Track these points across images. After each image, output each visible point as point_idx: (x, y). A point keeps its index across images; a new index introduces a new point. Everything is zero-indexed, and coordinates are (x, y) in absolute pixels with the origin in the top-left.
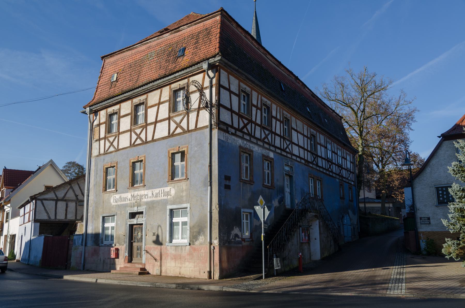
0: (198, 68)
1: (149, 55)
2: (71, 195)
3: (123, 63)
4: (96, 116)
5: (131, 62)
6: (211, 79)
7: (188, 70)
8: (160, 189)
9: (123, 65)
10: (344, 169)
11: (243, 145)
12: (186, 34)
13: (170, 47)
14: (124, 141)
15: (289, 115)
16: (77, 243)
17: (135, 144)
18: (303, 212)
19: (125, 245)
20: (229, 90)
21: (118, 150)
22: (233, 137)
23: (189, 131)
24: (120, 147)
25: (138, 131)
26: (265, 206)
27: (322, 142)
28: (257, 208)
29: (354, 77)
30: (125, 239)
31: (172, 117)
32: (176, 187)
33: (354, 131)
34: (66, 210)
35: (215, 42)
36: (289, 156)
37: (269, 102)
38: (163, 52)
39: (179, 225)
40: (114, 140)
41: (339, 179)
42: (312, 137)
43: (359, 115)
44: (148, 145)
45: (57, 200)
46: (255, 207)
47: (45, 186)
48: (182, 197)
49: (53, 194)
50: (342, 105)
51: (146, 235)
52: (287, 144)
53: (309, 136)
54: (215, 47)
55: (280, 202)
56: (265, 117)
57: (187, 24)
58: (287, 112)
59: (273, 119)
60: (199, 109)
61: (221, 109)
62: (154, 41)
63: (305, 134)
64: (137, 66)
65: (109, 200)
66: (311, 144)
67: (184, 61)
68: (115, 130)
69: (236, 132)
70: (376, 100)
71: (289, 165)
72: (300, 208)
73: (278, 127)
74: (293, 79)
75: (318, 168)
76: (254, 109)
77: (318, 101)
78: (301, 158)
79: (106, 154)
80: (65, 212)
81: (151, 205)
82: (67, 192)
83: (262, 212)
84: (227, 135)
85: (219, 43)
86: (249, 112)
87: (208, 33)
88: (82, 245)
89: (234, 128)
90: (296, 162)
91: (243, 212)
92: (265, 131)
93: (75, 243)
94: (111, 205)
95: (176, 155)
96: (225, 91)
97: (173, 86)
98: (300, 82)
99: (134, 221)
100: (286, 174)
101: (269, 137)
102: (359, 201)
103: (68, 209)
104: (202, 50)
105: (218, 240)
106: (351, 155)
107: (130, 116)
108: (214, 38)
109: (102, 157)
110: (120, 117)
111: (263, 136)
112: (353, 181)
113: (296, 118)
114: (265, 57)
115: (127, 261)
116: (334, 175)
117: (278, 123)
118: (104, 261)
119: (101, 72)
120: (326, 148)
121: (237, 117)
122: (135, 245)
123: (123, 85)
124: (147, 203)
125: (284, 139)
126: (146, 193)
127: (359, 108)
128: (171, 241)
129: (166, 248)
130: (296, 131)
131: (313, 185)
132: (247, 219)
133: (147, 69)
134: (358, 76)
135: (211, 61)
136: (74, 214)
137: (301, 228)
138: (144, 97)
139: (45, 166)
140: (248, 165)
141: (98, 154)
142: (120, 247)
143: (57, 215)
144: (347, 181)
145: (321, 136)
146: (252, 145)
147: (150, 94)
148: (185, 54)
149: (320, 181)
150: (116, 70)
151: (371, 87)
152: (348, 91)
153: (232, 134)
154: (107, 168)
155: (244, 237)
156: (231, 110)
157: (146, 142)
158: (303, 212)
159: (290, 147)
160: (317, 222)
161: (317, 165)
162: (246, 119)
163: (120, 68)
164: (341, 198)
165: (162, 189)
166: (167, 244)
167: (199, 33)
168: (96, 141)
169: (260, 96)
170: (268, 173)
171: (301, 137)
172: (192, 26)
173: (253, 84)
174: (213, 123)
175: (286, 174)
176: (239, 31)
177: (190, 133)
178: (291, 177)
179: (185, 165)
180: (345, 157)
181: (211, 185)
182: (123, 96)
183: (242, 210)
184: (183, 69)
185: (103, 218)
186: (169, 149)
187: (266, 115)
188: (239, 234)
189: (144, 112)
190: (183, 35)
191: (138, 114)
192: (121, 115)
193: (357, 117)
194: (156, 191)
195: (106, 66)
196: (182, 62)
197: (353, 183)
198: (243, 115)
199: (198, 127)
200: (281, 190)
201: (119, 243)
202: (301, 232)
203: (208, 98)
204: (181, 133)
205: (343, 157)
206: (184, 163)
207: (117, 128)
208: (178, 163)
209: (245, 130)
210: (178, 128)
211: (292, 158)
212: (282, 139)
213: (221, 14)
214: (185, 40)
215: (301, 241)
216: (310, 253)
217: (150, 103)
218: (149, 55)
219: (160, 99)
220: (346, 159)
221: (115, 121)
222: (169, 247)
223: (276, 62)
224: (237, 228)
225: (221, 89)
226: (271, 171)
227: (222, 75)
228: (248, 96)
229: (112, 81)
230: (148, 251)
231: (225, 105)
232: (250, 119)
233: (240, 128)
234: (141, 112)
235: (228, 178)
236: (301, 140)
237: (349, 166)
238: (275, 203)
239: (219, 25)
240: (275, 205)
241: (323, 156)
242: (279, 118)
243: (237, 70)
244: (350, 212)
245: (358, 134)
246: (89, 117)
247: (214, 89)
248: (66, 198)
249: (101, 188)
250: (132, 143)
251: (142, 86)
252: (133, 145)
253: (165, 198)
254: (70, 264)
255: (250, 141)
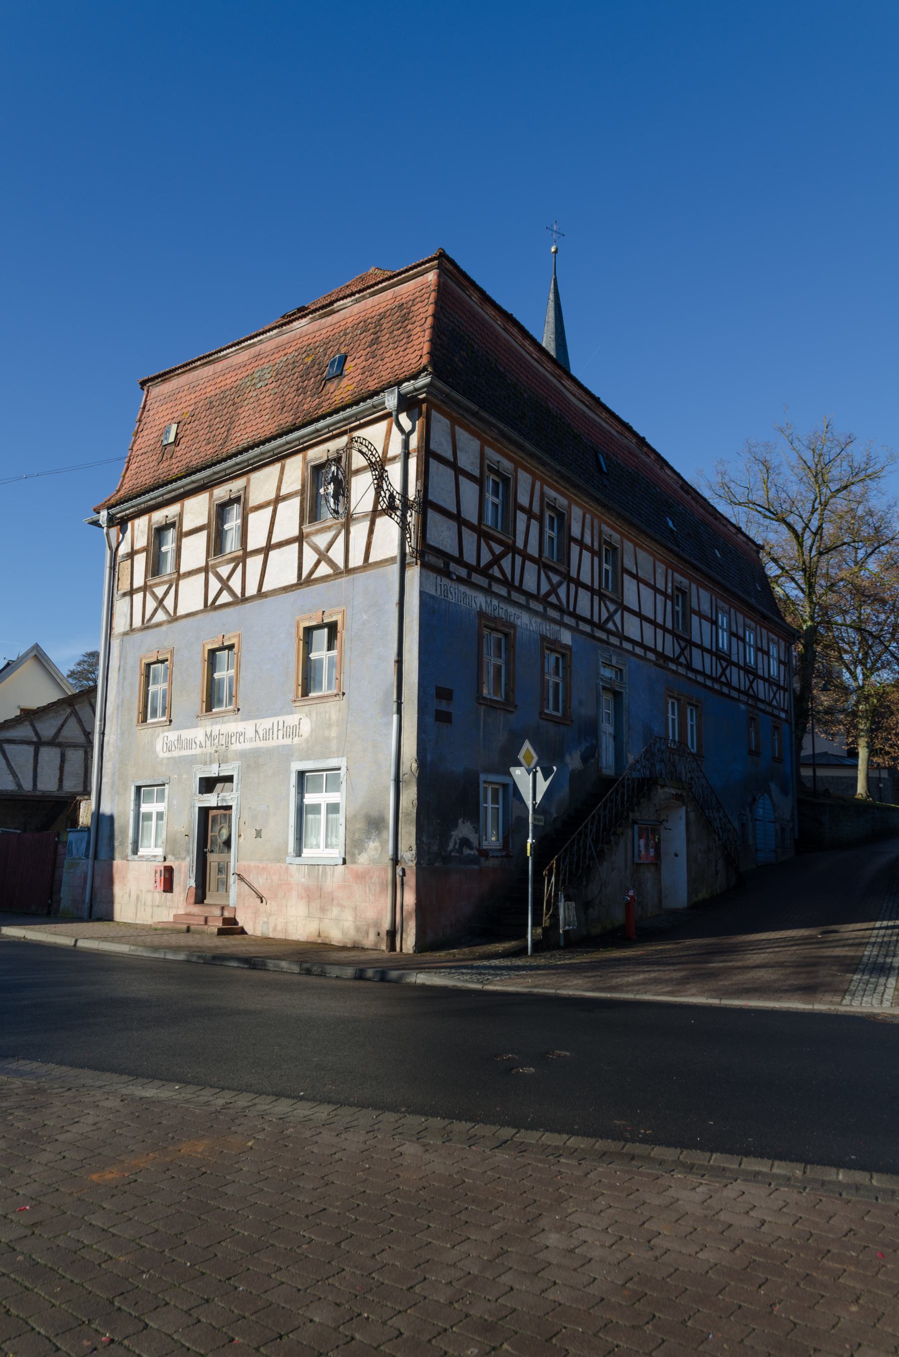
0: (374, 407)
1: (256, 375)
2: (72, 732)
3: (193, 396)
4: (124, 534)
5: (213, 393)
6: (407, 435)
7: (349, 412)
8: (275, 720)
9: (192, 401)
10: (762, 678)
11: (489, 611)
12: (350, 320)
13: (308, 356)
14: (191, 595)
15: (616, 536)
16: (74, 852)
17: (217, 603)
18: (644, 787)
19: (188, 859)
20: (453, 464)
21: (174, 618)
22: (463, 588)
23: (348, 571)
24: (181, 612)
25: (224, 571)
26: (538, 769)
27: (705, 608)
28: (518, 773)
29: (796, 443)
30: (188, 843)
31: (308, 535)
32: (314, 715)
33: (793, 585)
34: (61, 769)
35: (421, 339)
36: (614, 640)
37: (562, 501)
38: (290, 367)
39: (319, 813)
40: (166, 593)
41: (746, 703)
42: (679, 595)
43: (808, 543)
44: (248, 606)
45: (38, 744)
46: (512, 769)
47: (22, 710)
48: (328, 740)
49: (30, 728)
50: (765, 516)
51: (240, 836)
52: (608, 610)
53: (669, 591)
54: (419, 353)
55: (585, 759)
56: (551, 539)
57: (353, 294)
58: (613, 528)
59: (572, 544)
60: (375, 514)
61: (431, 513)
62: (271, 338)
63: (658, 586)
64: (227, 403)
65: (152, 745)
66: (674, 613)
67: (342, 390)
68: (169, 567)
69: (469, 576)
70: (853, 505)
71: (614, 663)
72: (635, 775)
73: (585, 566)
74: (632, 443)
75: (691, 675)
76: (521, 518)
77: (697, 502)
78: (646, 648)
79: (148, 628)
80: (57, 772)
81: (253, 760)
82: (63, 725)
83: (530, 784)
84: (445, 581)
85: (431, 341)
86: (509, 526)
87: (405, 318)
88: (87, 856)
89: (466, 565)
90: (633, 658)
91: (485, 782)
92: (550, 574)
93: (70, 852)
94: (157, 757)
95: (316, 633)
96: (441, 466)
97: (312, 453)
98: (649, 452)
99: (211, 800)
100: (604, 688)
101: (562, 591)
102: (799, 763)
103: (67, 767)
104: (386, 360)
105: (414, 852)
106: (782, 643)
107: (205, 533)
108: (418, 329)
109: (138, 636)
110: (181, 535)
111: (545, 588)
112: (783, 710)
113: (636, 544)
114: (559, 385)
115: (192, 900)
116: (735, 694)
117: (586, 555)
118: (138, 897)
119: (140, 421)
120: (714, 622)
121: (475, 536)
122: (213, 859)
123: (192, 453)
124: (243, 755)
125: (602, 597)
126: (239, 730)
127: (807, 526)
128: (299, 854)
129: (287, 868)
130: (635, 576)
131: (676, 717)
132: (495, 800)
133: (251, 412)
134: (806, 442)
135: (407, 387)
136: (82, 780)
137: (636, 827)
138: (239, 483)
139: (21, 660)
140: (500, 662)
141: (128, 628)
142: (177, 863)
143: (38, 781)
144: (769, 709)
145: (702, 591)
146: (512, 610)
147: (255, 476)
148: (346, 373)
149: (696, 707)
150: (176, 415)
151: (838, 472)
152: (780, 481)
153: (460, 580)
154: (148, 665)
155: (485, 845)
156: (457, 518)
157: (244, 599)
158: (644, 787)
159: (617, 618)
160: (682, 811)
161: (689, 667)
162: (500, 542)
163: (185, 411)
164: (751, 752)
165: (280, 719)
166: (289, 860)
167: (383, 316)
168: (124, 595)
169: (538, 485)
170: (557, 685)
171: (646, 592)
172: (364, 298)
173: (520, 453)
174: (408, 550)
175: (604, 688)
176: (487, 314)
177: (351, 577)
178: (617, 695)
179: (337, 660)
180: (765, 649)
181: (399, 711)
182: (189, 479)
183: (483, 777)
184: (336, 411)
185: (138, 788)
186: (297, 618)
187: (554, 535)
188: (473, 838)
189: (239, 521)
190: (344, 322)
191: (226, 527)
192: (185, 528)
193: (801, 545)
194: (266, 724)
195: (152, 405)
196: (337, 393)
197: (783, 715)
198: (491, 532)
199: (371, 560)
200: (591, 729)
201: (173, 855)
202: (636, 836)
203: (397, 486)
204: (328, 576)
205: (759, 649)
206: (334, 653)
207: (174, 563)
208: (320, 653)
209: (496, 572)
210: (323, 564)
211: (620, 648)
212: (596, 598)
213: (439, 267)
214: (345, 334)
215: (637, 860)
216: (660, 891)
217: (254, 499)
218: (256, 375)
219: (279, 488)
220: (767, 653)
221: (168, 547)
222: (293, 868)
223: (586, 399)
224: (468, 824)
225: (433, 463)
226: (564, 678)
227: (434, 425)
228: (506, 484)
229: (165, 443)
230: (244, 875)
231: (441, 503)
232: (510, 542)
233: (483, 564)
234: (233, 524)
235: (444, 694)
236: (649, 603)
237: (774, 671)
238: (574, 761)
239: (433, 295)
240: (571, 767)
241: (707, 644)
242: (590, 544)
243: (475, 414)
244: (773, 786)
245: (803, 592)
246: (108, 534)
247: (413, 462)
248: (60, 739)
249: (135, 714)
250: (210, 602)
251: (235, 455)
252: (211, 607)
253: (287, 741)
254: (59, 902)
255: (508, 600)
